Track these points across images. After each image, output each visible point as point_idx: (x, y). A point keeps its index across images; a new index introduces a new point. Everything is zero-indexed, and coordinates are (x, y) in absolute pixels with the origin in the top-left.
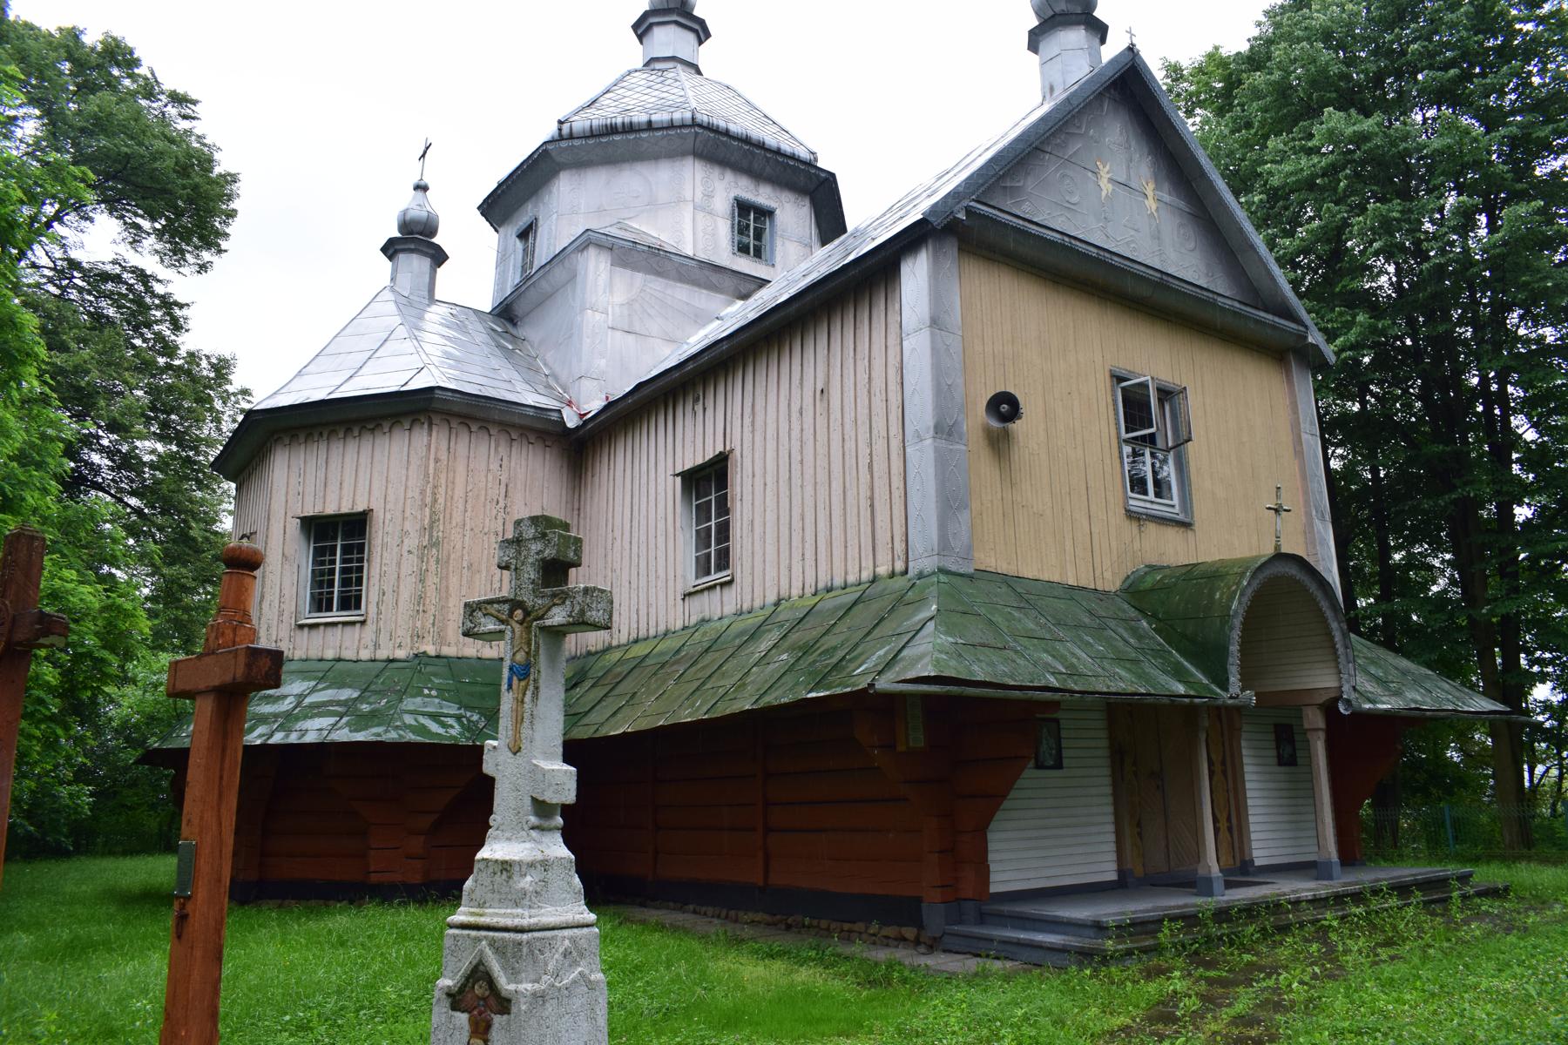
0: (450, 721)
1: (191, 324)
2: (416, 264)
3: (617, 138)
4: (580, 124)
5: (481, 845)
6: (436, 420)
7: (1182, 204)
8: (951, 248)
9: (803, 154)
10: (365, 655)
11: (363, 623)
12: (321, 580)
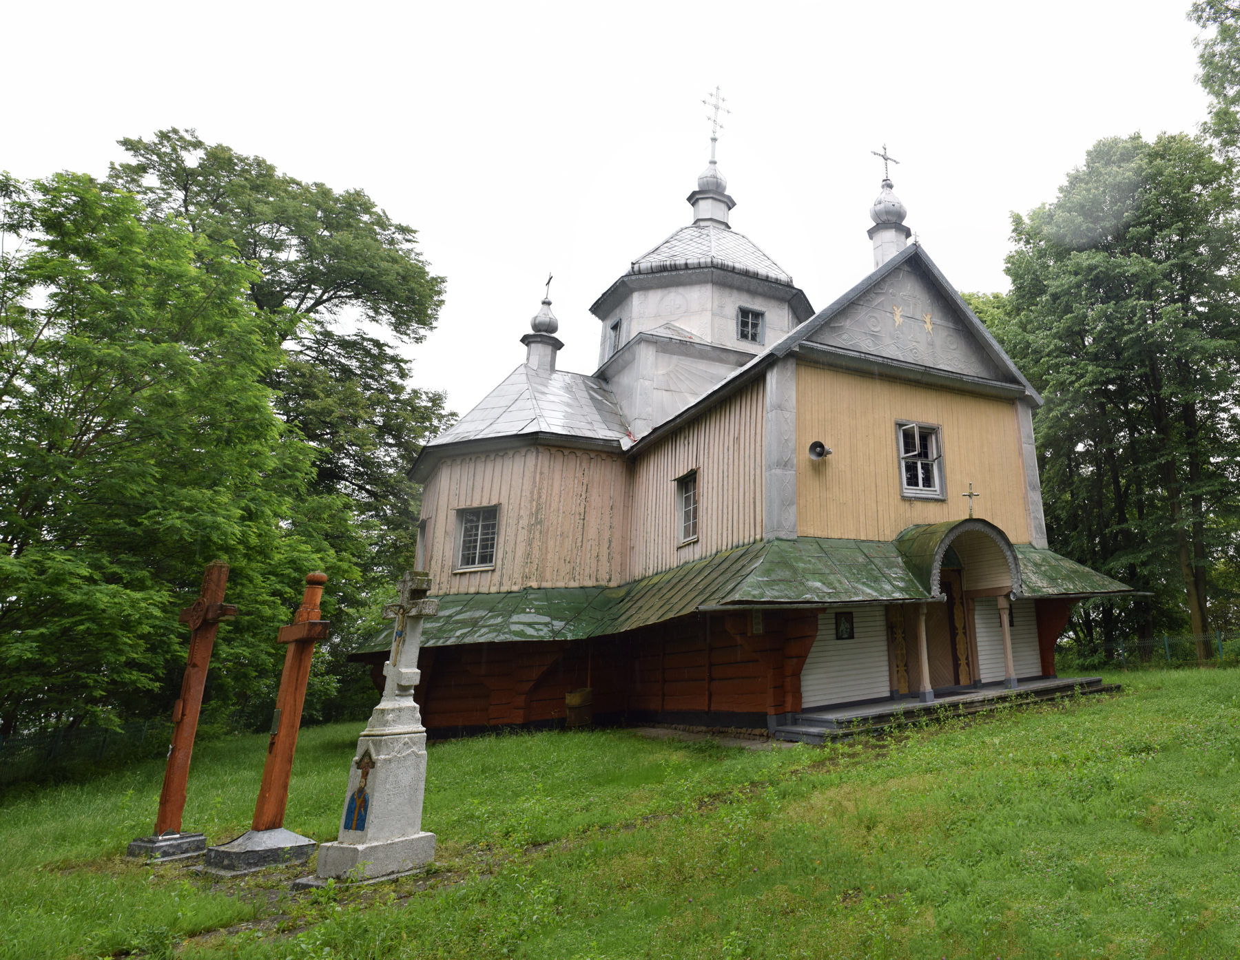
0: (541, 627)
1: (413, 373)
2: (540, 350)
3: (665, 274)
4: (645, 265)
5: (378, 703)
6: (541, 449)
7: (951, 325)
8: (791, 365)
9: (783, 278)
10: (494, 590)
11: (493, 571)
12: (469, 545)
